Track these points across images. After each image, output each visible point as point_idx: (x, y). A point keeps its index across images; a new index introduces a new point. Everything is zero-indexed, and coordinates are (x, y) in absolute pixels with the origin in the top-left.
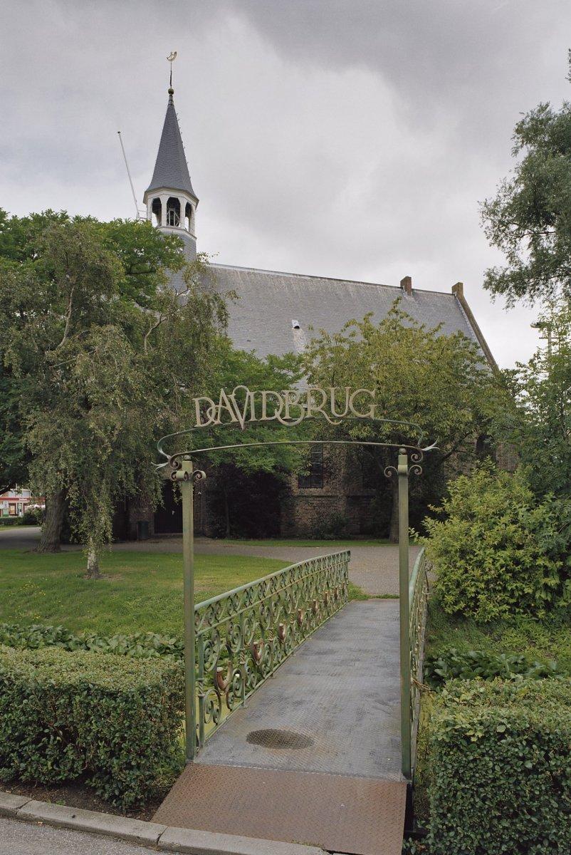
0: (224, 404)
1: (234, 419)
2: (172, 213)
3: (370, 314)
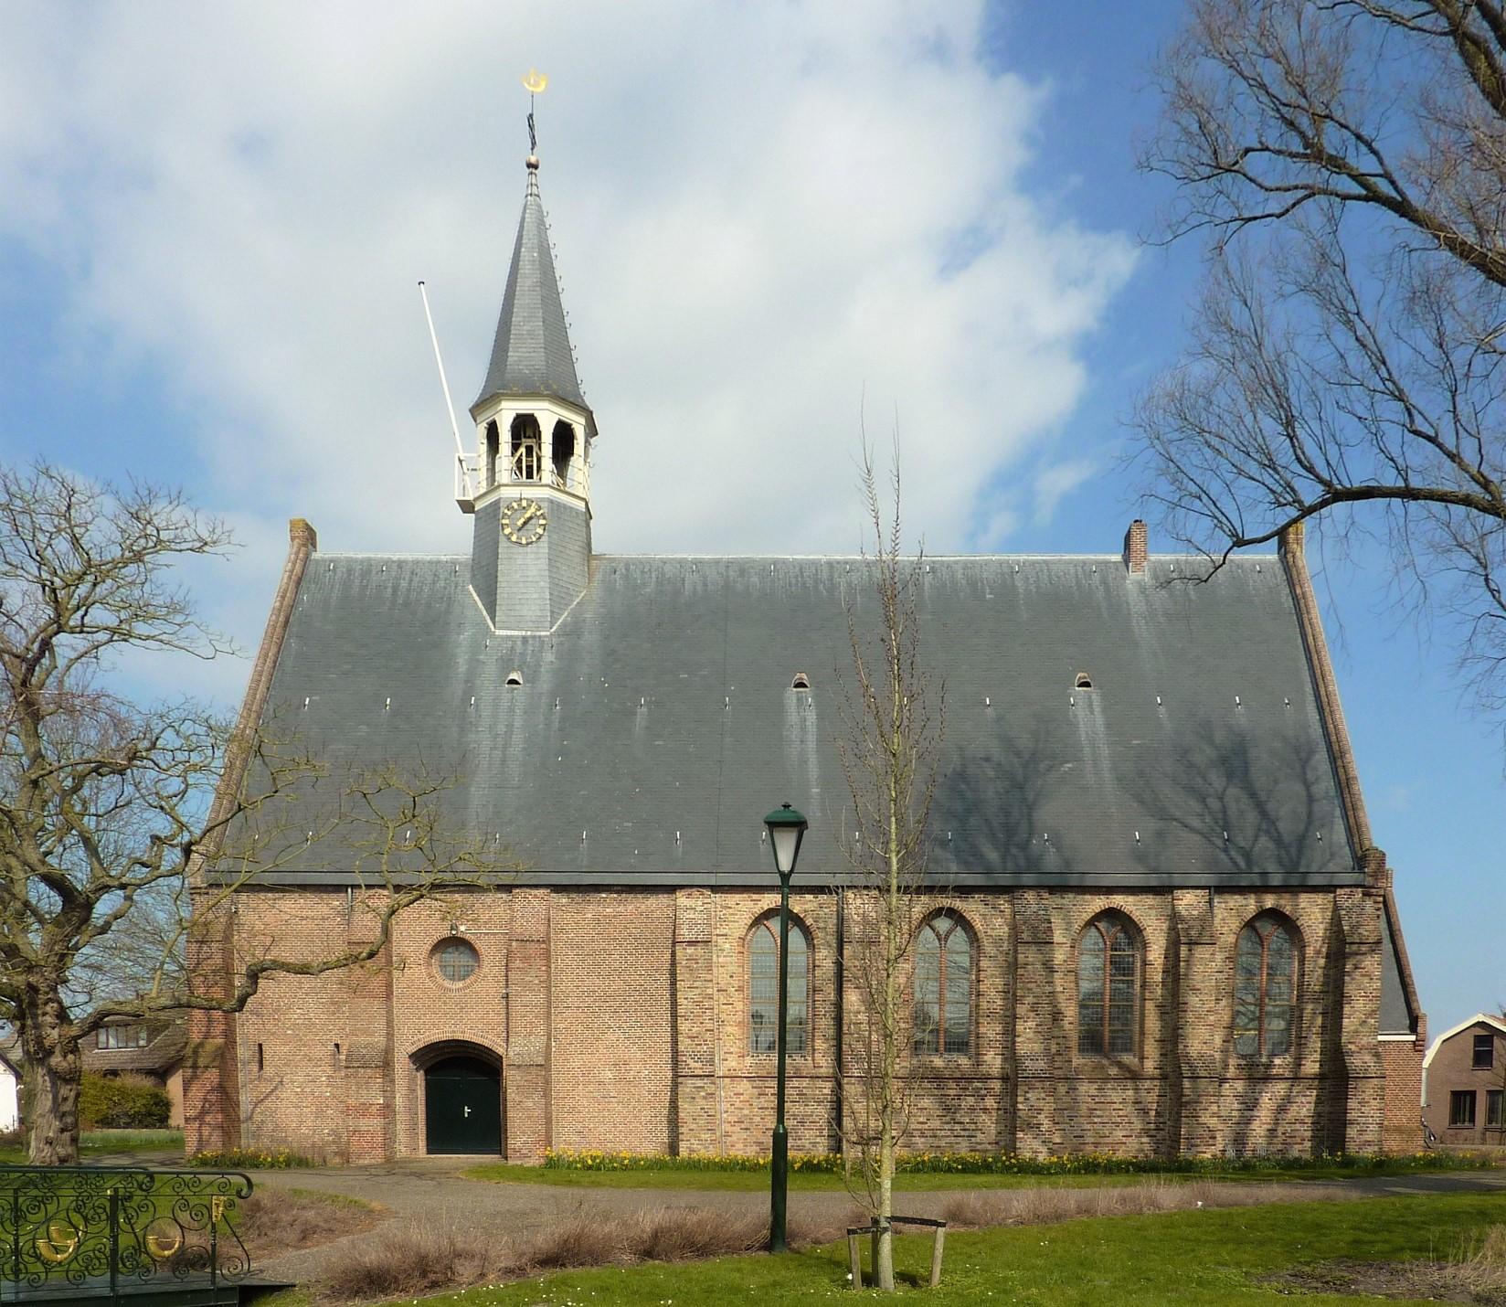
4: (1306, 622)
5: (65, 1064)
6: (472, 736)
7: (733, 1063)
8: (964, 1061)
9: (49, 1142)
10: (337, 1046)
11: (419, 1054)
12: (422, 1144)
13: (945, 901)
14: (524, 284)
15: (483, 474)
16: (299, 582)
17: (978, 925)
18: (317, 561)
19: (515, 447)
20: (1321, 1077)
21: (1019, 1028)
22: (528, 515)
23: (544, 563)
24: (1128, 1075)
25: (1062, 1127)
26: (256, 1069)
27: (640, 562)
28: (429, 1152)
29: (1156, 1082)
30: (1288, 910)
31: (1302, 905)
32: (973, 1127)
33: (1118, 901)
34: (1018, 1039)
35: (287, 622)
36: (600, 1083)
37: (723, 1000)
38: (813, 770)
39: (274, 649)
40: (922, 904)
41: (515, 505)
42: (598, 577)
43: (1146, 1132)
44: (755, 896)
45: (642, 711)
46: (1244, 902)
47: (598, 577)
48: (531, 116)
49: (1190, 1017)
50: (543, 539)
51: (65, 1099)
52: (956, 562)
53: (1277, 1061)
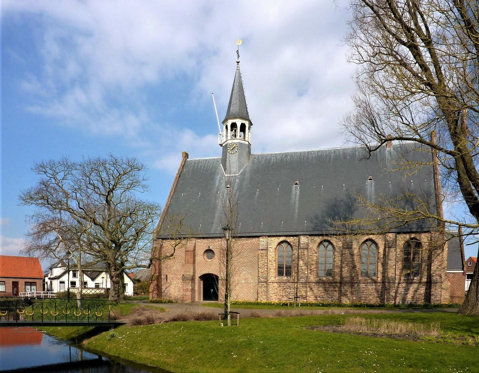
5: (116, 280)
6: (217, 201)
7: (273, 279)
8: (331, 278)
9: (113, 297)
10: (183, 275)
11: (203, 277)
12: (202, 298)
13: (326, 238)
14: (235, 91)
15: (225, 137)
16: (183, 167)
17: (334, 244)
18: (188, 161)
19: (232, 130)
20: (427, 282)
21: (343, 270)
22: (234, 147)
23: (237, 158)
24: (373, 282)
25: (355, 295)
26: (166, 280)
27: (262, 155)
28: (204, 300)
29: (381, 284)
30: (418, 238)
31: (422, 236)
32: (332, 295)
33: (371, 236)
34: (343, 273)
35: (180, 176)
37: (270, 263)
38: (297, 206)
39: (176, 183)
40: (318, 239)
41: (231, 144)
42: (251, 160)
43: (378, 297)
44: (279, 238)
45: (257, 193)
46: (405, 236)
47: (251, 160)
48: (238, 51)
49: (389, 267)
50: (237, 152)
51: (116, 287)
52: (341, 149)
53: (415, 278)
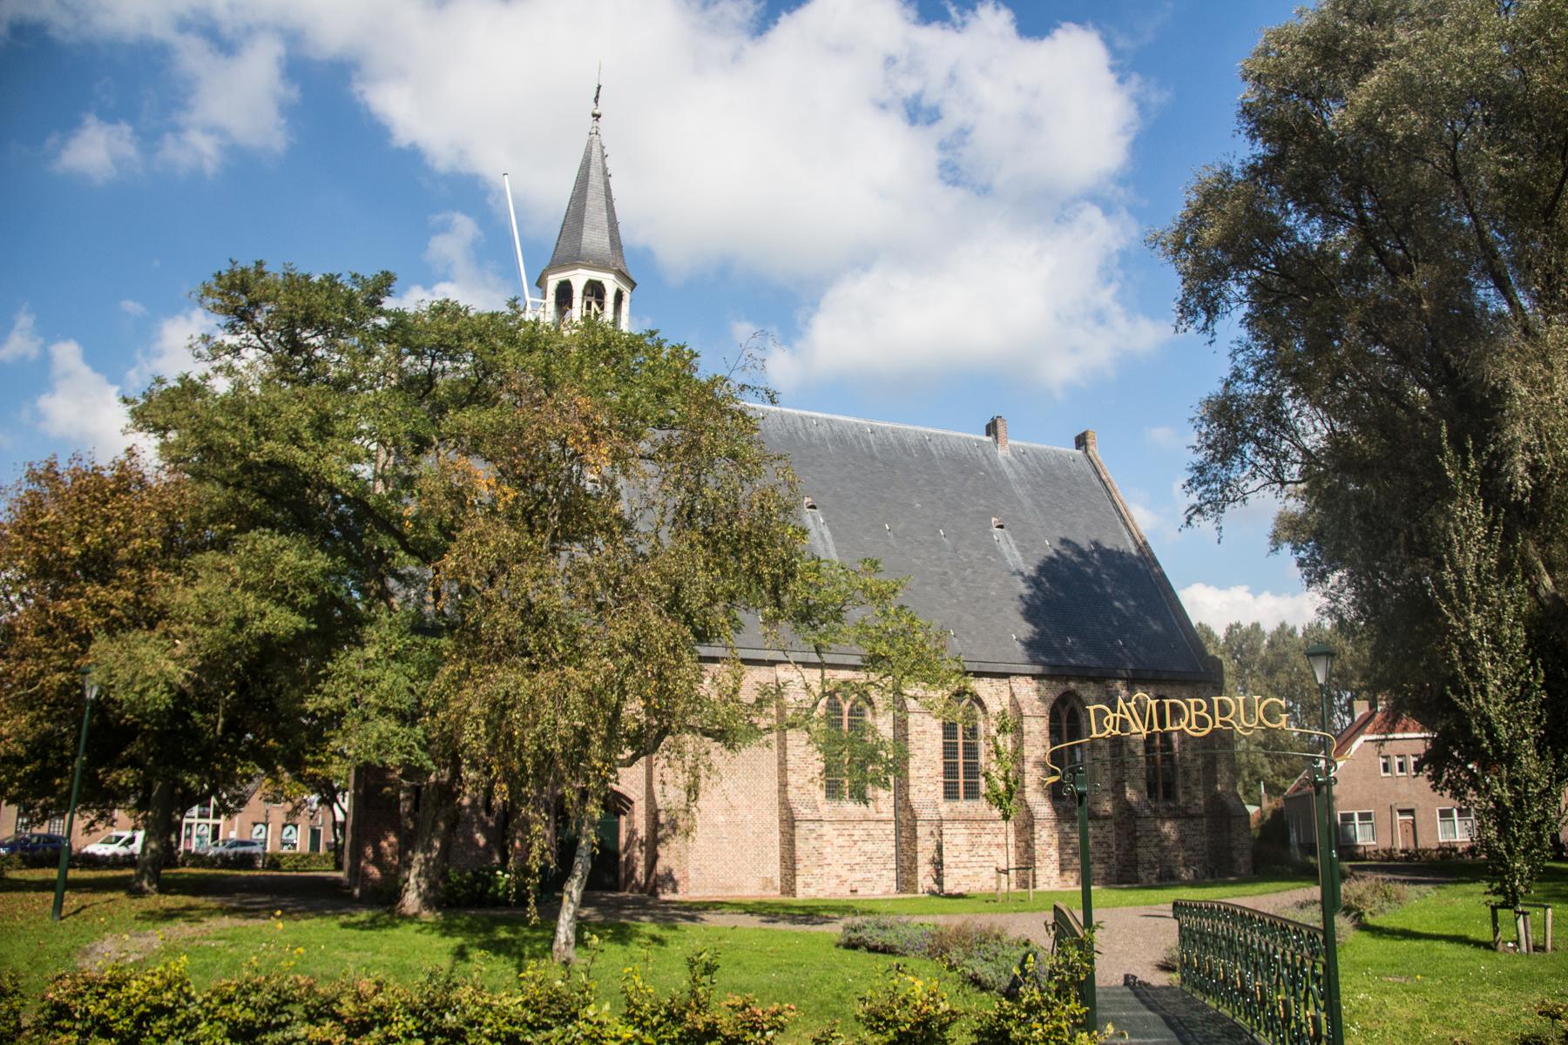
0: (1122, 712)
1: (1135, 729)
2: (589, 306)
3: (1210, 342)
4: (1116, 498)
36: (714, 825)
